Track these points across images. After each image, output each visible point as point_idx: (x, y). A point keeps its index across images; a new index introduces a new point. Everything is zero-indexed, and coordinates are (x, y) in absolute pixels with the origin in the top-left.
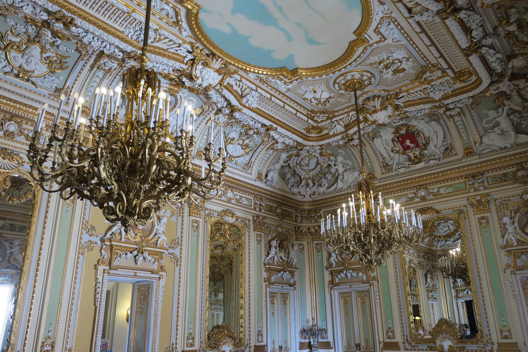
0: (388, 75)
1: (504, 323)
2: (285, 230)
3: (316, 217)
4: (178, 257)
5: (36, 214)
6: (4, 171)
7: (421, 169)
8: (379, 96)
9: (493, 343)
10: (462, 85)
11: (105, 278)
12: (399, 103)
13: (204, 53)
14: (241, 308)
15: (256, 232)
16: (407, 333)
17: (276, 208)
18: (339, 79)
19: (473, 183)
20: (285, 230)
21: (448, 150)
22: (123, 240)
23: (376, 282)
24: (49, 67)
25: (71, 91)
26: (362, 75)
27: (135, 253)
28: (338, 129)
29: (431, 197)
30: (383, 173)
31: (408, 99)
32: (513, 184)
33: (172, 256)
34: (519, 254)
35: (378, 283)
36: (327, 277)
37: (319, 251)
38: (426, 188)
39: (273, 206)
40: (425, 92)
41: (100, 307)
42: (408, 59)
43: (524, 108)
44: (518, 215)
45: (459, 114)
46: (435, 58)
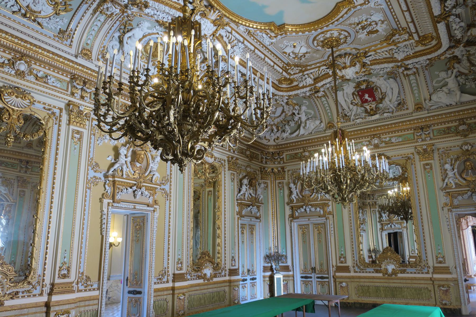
0: (363, 35)
1: (439, 251)
2: (252, 170)
3: (279, 160)
4: (168, 192)
5: (48, 150)
6: (17, 109)
8: (350, 54)
9: (429, 267)
10: (423, 48)
11: (110, 210)
12: (366, 61)
13: (203, 4)
14: (218, 237)
15: (230, 171)
16: (356, 258)
17: (246, 150)
18: (319, 37)
19: (421, 134)
20: (252, 170)
21: (401, 104)
22: (124, 176)
23: (332, 216)
24: (54, 8)
25: (74, 34)
26: (340, 34)
27: (135, 188)
28: (308, 82)
29: (383, 145)
31: (375, 58)
32: (455, 136)
33: (163, 192)
34: (456, 195)
35: (333, 217)
36: (288, 211)
37: (281, 189)
38: (379, 137)
39: (244, 149)
41: (106, 236)
42: (383, 22)
43: (470, 72)
44: (458, 162)
45: (415, 73)
46: (407, 22)
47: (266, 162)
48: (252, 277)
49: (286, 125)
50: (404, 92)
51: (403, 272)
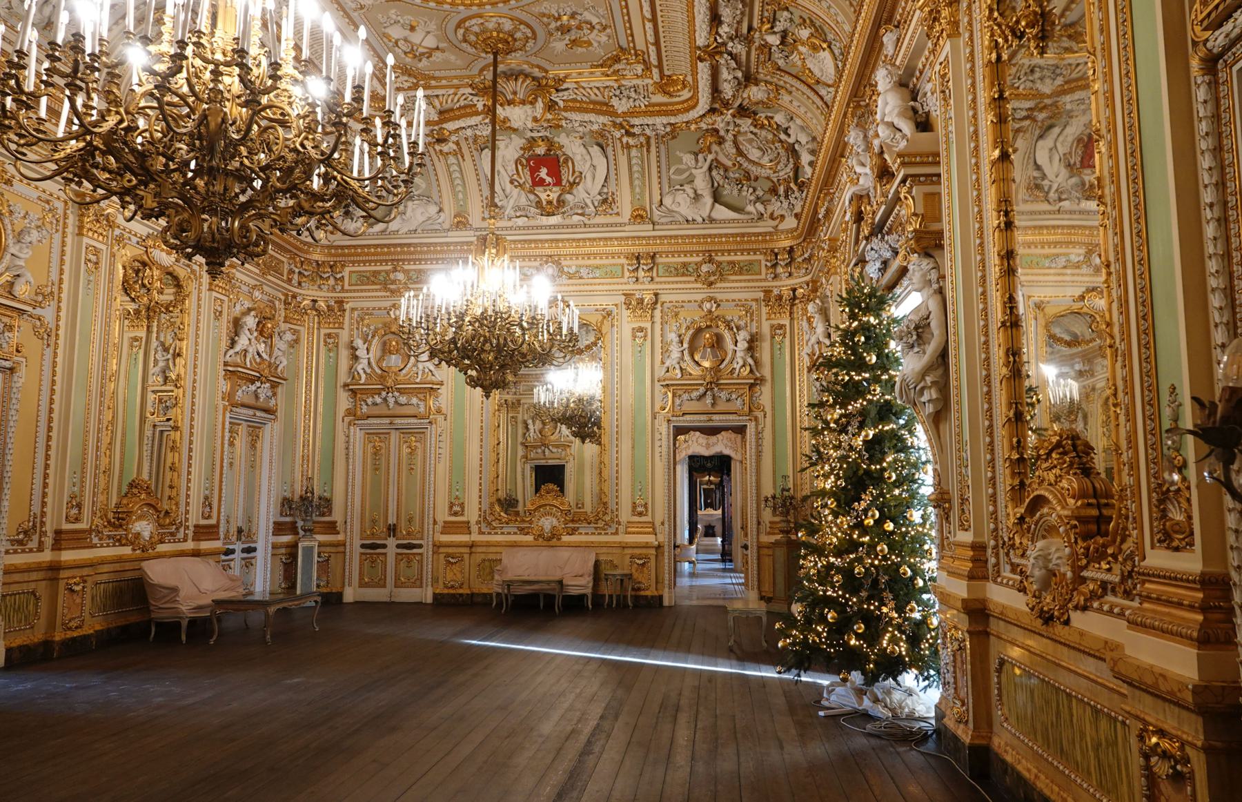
2: (266, 298)
7: (554, 226)
9: (619, 523)
10: (665, 99)
15: (214, 294)
18: (474, 21)
20: (266, 298)
30: (484, 219)
37: (330, 350)
40: (606, 94)
43: (734, 165)
47: (300, 284)
48: (246, 546)
50: (617, 180)
51: (573, 532)
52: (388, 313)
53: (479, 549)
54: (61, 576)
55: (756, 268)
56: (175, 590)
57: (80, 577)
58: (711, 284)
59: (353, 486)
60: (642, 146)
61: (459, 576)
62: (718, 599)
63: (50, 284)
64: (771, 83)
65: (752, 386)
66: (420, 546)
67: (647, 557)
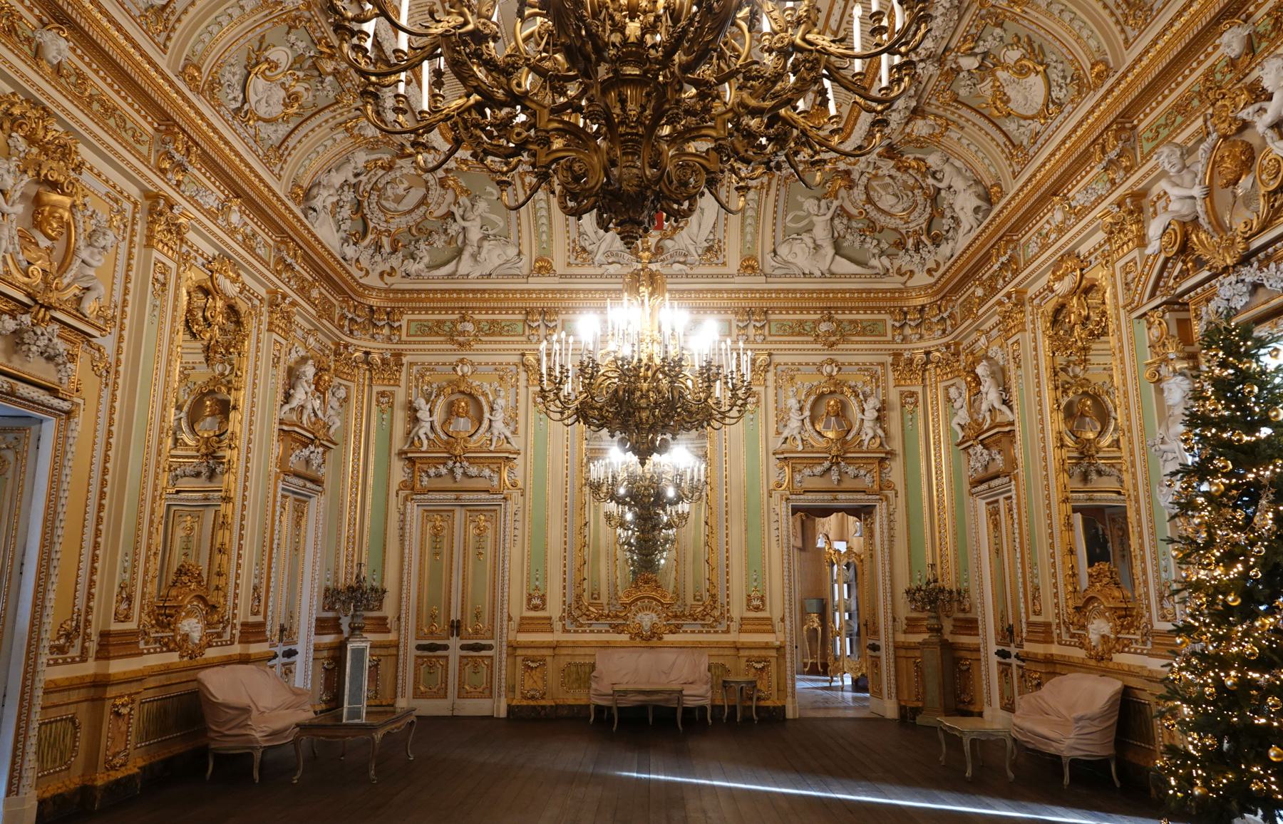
2: (318, 345)
9: (730, 619)
15: (275, 336)
16: (570, 599)
30: (569, 264)
39: (307, 280)
47: (351, 332)
48: (286, 648)
49: (421, 242)
50: (725, 225)
51: (676, 629)
52: (454, 369)
53: (564, 651)
54: (108, 695)
55: (880, 328)
56: (245, 710)
57: (129, 695)
58: (832, 345)
59: (409, 573)
60: (762, 187)
61: (540, 683)
62: (819, 708)
63: (112, 305)
64: (941, 117)
65: (882, 460)
66: (490, 647)
67: (764, 659)
